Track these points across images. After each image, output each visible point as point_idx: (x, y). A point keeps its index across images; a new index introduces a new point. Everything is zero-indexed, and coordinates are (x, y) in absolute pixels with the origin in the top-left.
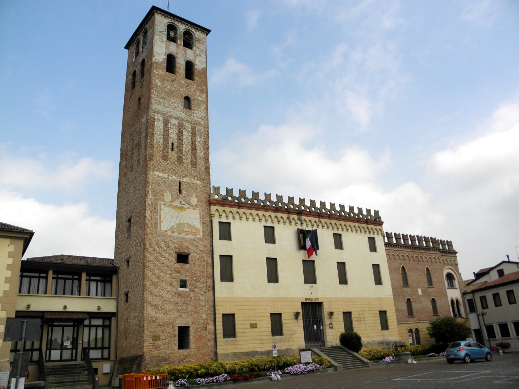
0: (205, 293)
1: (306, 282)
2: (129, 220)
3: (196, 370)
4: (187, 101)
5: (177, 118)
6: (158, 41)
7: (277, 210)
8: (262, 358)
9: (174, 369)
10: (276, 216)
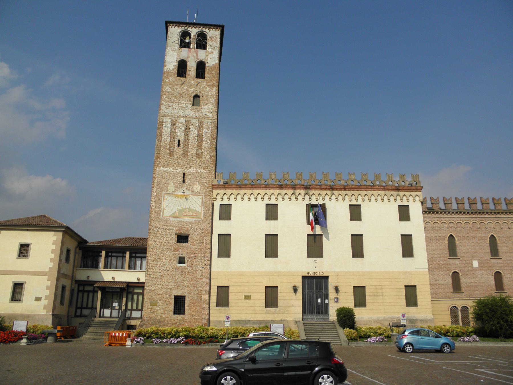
5: (185, 117)
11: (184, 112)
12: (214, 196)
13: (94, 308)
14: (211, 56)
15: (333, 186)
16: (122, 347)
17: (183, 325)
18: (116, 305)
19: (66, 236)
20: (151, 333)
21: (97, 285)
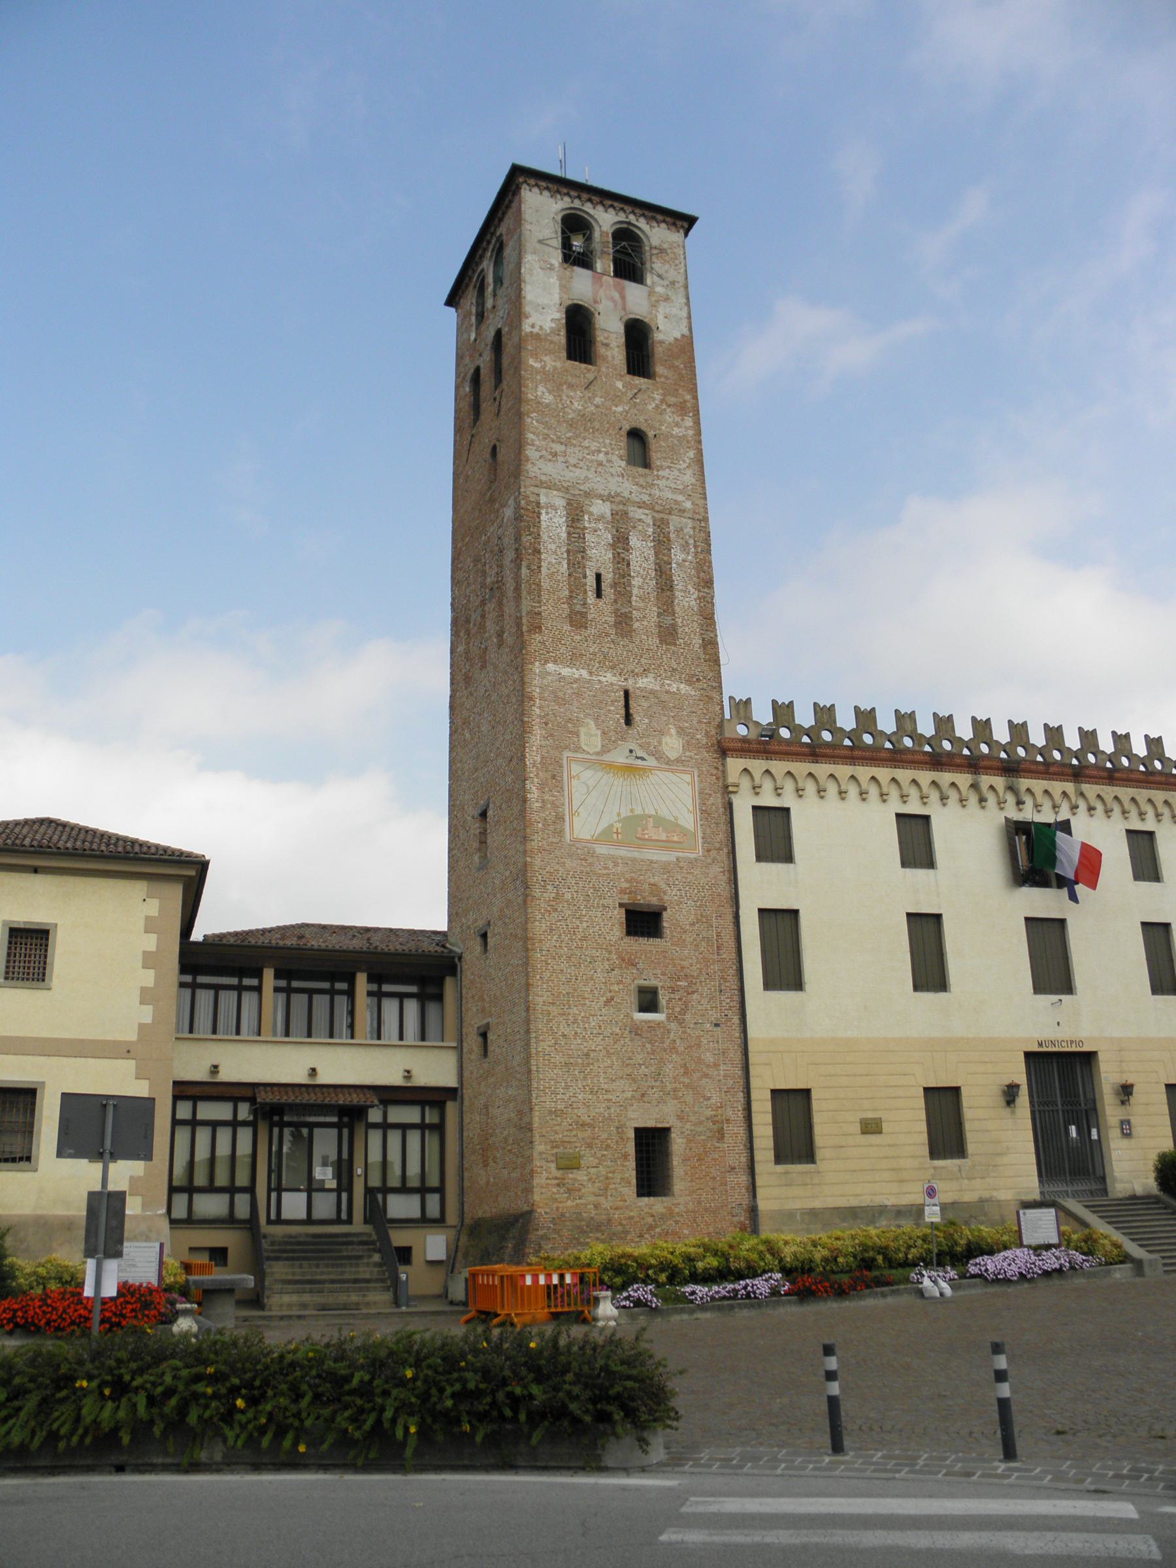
0: (717, 1025)
1: (1038, 989)
2: (484, 815)
3: (689, 1259)
4: (637, 445)
5: (609, 498)
6: (537, 271)
7: (937, 761)
8: (899, 1226)
9: (623, 1256)
10: (933, 782)
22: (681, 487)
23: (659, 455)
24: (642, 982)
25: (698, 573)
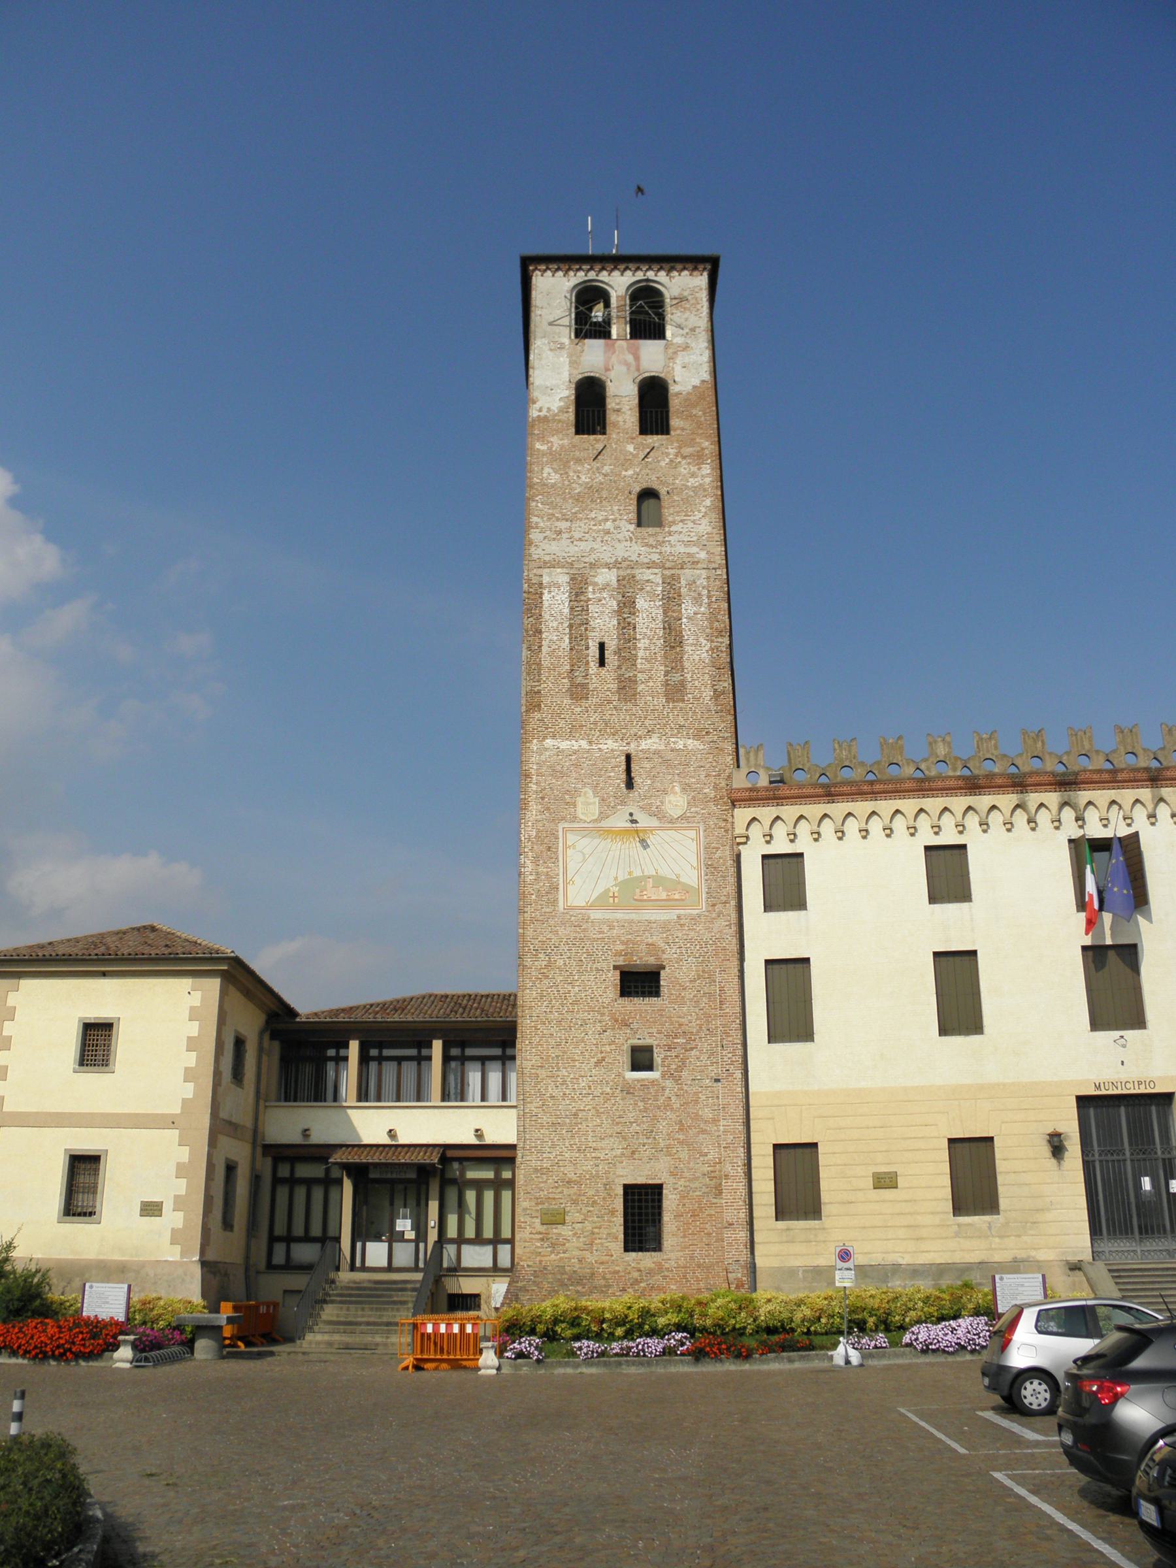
0: (717, 1080)
5: (617, 565)
11: (613, 547)
12: (740, 829)
13: (329, 1239)
14: (684, 357)
15: (1158, 770)
16: (457, 1375)
17: (661, 1289)
18: (404, 1225)
19: (232, 989)
20: (556, 1321)
21: (338, 1157)
22: (695, 539)
23: (671, 510)
24: (636, 1042)
25: (711, 623)
